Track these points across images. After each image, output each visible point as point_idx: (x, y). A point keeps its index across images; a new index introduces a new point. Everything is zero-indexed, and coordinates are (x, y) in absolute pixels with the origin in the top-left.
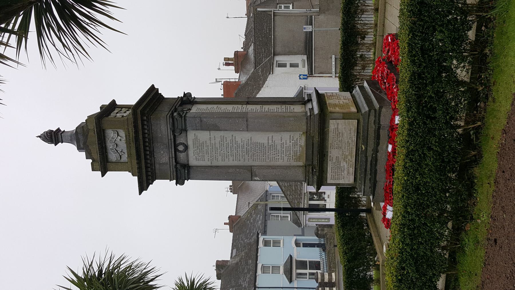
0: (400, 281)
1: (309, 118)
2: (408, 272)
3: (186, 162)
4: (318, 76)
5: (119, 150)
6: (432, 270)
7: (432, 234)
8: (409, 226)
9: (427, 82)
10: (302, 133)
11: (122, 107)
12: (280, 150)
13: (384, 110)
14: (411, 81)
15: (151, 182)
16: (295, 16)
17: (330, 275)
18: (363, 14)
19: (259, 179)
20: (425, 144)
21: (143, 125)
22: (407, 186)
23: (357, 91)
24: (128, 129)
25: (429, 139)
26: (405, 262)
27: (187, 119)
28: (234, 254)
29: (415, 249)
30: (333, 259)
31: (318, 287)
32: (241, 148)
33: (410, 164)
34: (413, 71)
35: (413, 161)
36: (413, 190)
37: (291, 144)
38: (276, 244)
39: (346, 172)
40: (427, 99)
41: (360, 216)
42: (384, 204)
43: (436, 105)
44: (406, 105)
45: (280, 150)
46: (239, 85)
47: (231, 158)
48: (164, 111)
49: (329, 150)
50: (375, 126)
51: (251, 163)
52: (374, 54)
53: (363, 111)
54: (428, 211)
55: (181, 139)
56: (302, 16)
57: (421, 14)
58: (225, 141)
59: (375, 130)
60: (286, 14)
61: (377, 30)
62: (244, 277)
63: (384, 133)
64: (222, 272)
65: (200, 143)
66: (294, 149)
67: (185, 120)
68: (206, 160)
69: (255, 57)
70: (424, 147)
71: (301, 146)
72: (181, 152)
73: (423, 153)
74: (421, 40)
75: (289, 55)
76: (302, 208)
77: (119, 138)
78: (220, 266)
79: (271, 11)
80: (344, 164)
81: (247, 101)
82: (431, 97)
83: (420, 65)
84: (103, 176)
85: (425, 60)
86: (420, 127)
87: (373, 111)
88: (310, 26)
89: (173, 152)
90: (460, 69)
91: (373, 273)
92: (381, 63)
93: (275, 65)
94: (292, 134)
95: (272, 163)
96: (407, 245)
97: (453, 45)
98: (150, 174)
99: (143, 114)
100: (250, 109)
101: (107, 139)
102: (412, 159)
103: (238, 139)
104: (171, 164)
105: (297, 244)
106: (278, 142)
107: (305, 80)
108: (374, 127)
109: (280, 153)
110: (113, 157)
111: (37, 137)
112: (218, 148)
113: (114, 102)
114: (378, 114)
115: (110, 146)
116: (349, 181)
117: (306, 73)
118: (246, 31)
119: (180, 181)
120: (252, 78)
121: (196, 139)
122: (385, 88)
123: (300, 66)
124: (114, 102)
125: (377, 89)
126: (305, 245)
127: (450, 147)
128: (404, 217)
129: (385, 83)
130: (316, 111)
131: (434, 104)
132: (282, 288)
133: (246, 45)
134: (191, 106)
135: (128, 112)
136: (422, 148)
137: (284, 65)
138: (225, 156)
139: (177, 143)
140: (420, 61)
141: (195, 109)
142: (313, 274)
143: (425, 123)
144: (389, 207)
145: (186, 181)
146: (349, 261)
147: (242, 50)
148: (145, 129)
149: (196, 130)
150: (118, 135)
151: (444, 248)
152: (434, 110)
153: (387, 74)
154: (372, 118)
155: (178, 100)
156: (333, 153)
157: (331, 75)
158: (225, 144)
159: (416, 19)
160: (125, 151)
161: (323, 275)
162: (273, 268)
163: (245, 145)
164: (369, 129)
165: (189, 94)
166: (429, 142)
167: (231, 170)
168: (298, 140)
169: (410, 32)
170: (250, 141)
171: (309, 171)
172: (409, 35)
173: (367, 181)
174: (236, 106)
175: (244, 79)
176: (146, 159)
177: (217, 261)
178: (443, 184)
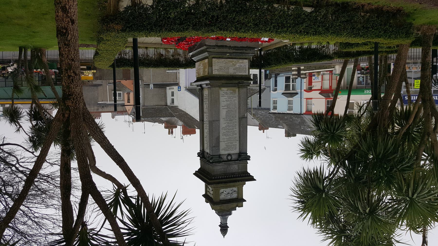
0: (307, 33)
1: (212, 86)
2: (303, 29)
3: (238, 154)
4: (179, 80)
5: (231, 192)
6: (301, 15)
7: (281, 16)
8: (277, 29)
9: (198, 21)
10: (220, 90)
11: (206, 191)
12: (230, 102)
13: (207, 44)
14: (197, 30)
15: (248, 174)
16: (144, 94)
17: (293, 71)
18: (149, 56)
19: (246, 114)
20: (232, 21)
21: (217, 179)
22: (255, 31)
23: (195, 59)
24: (220, 187)
25: (229, 19)
26: (297, 31)
27: (213, 154)
28: (281, 127)
29: (290, 25)
30: (284, 69)
31: (301, 77)
32: (229, 124)
33: (243, 29)
34: (192, 29)
35: (241, 27)
36: (257, 27)
37: (226, 96)
38: (275, 102)
39: (242, 64)
40: (207, 21)
41: (263, 54)
42: (259, 42)
43: (210, 16)
44: (210, 32)
45: (230, 102)
46: (184, 125)
47: (235, 129)
48: (209, 167)
49: (230, 74)
50: (216, 48)
51: (237, 118)
52: (171, 49)
53: (208, 55)
54: (269, 18)
55: (225, 158)
56: (144, 89)
57: (161, 26)
58: (225, 133)
59: (218, 48)
60: (143, 99)
61: (158, 48)
62: (295, 121)
63: (220, 43)
64: (292, 134)
65: (226, 147)
66: (229, 94)
67: (214, 156)
68: (236, 143)
69: (168, 117)
70: (233, 22)
71: (227, 90)
72: (231, 158)
73: (237, 22)
74: (175, 25)
75: (167, 97)
76: (259, 88)
77: (224, 192)
78: (288, 134)
79: (142, 108)
80: (237, 66)
81: (201, 121)
82: (206, 19)
83: (189, 25)
84: (246, 201)
85: (186, 23)
86: (223, 25)
87: (208, 50)
88: (150, 85)
89: (232, 162)
90: (190, 3)
91: (297, 47)
92: (179, 45)
93: (173, 105)
94: (221, 95)
95: (237, 106)
96: (287, 30)
97: (177, 7)
98: (244, 175)
99: (211, 179)
100: (206, 120)
101: (225, 199)
102: (240, 28)
103: (224, 125)
104: (238, 163)
105: (275, 90)
106: (225, 103)
107: (181, 87)
108: (217, 49)
109: (231, 102)
110: (235, 196)
111: (224, 237)
112: (229, 137)
113: (203, 196)
114: (210, 47)
115: (229, 197)
116: (246, 62)
117: (177, 87)
118: (152, 122)
119: (248, 158)
120: (180, 118)
121: (224, 149)
122: (194, 43)
123: (173, 90)
124: (203, 196)
125: (194, 47)
126: (276, 85)
127: (233, 7)
128: (272, 32)
129: (191, 43)
130: (208, 82)
131: (210, 16)
132: (301, 98)
133: (161, 122)
134: (205, 153)
135: (210, 187)
136: (234, 23)
137: (173, 100)
138: (233, 133)
139: (227, 160)
140: (186, 26)
141: (207, 150)
142: (293, 80)
143: (220, 22)
144: (262, 39)
145: (248, 155)
146: (291, 61)
147: (164, 124)
148: (229, 177)
149: (219, 149)
150: (223, 193)
151: (288, 9)
152: (213, 16)
153: (186, 42)
154: (211, 50)
155: (202, 159)
156: (232, 72)
157: (178, 72)
158: (227, 133)
159: (164, 28)
160: (231, 189)
161: (293, 75)
162: (289, 104)
163: (227, 122)
164: (218, 51)
165: (198, 153)
166: (230, 19)
167: (242, 129)
168: (224, 92)
169: (171, 31)
170: (225, 119)
171: (242, 85)
172: (172, 32)
173: (247, 52)
174: (205, 127)
175: (181, 123)
176: (236, 177)
177: (286, 136)
178: (254, 10)
